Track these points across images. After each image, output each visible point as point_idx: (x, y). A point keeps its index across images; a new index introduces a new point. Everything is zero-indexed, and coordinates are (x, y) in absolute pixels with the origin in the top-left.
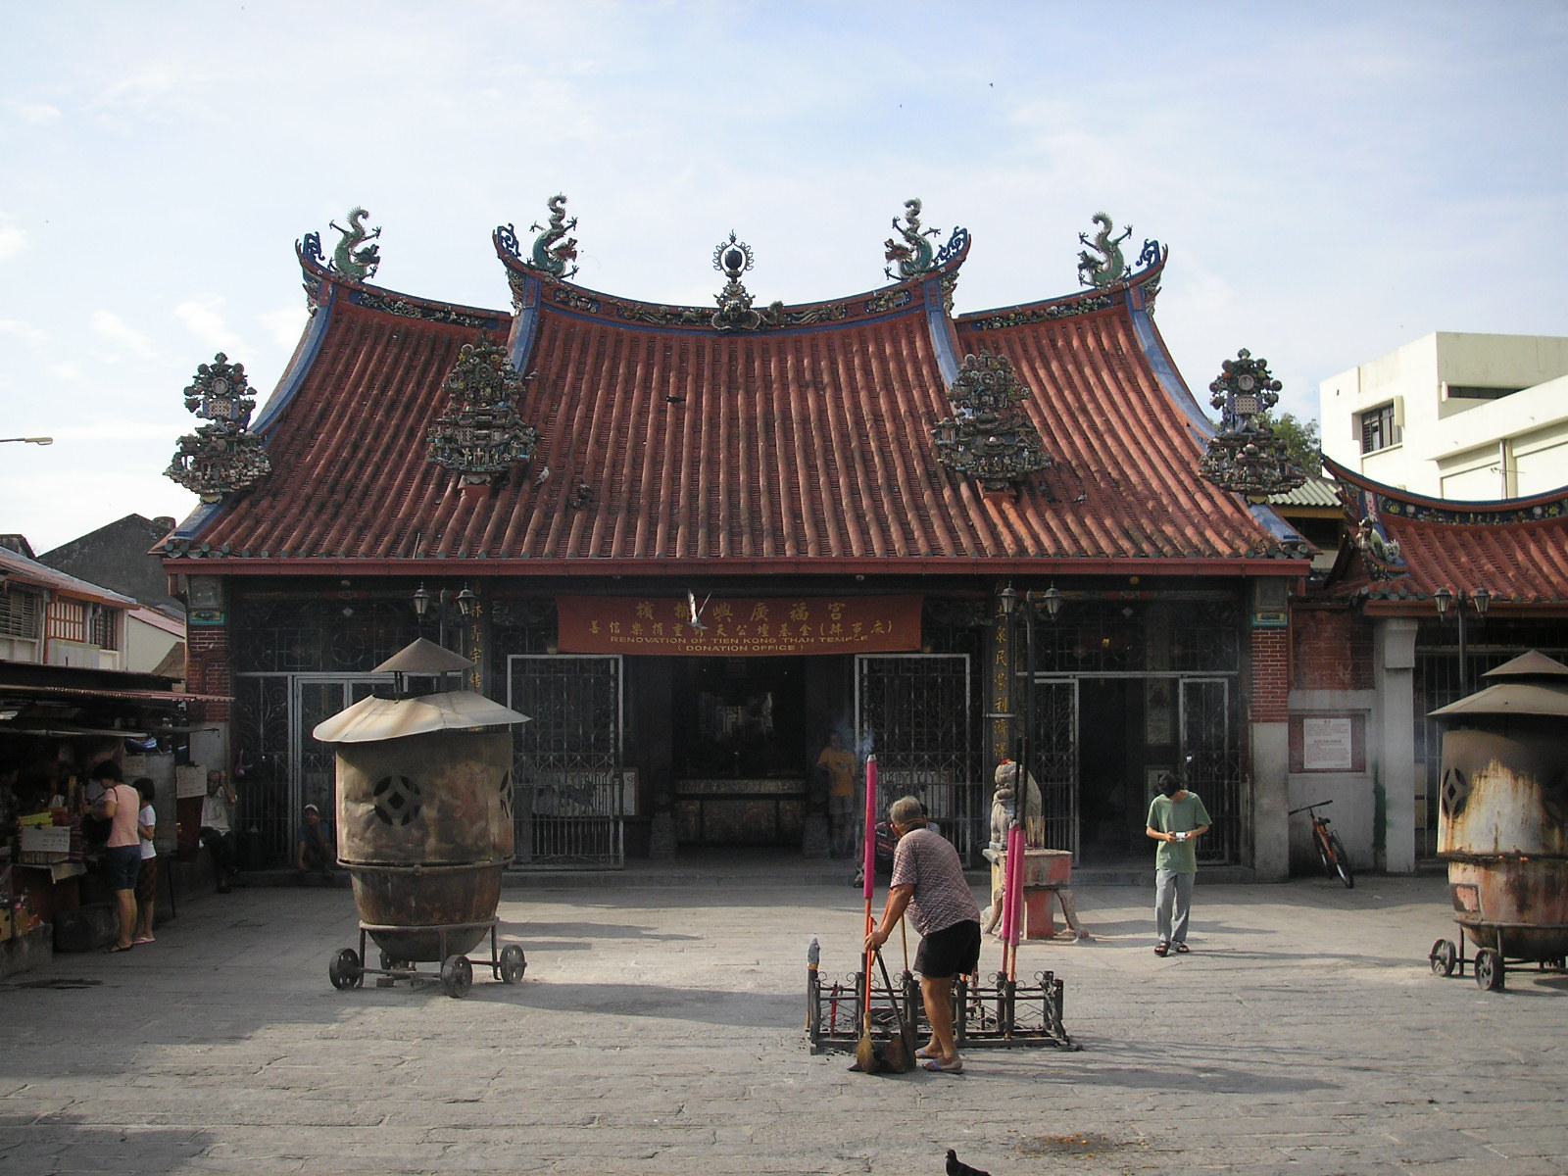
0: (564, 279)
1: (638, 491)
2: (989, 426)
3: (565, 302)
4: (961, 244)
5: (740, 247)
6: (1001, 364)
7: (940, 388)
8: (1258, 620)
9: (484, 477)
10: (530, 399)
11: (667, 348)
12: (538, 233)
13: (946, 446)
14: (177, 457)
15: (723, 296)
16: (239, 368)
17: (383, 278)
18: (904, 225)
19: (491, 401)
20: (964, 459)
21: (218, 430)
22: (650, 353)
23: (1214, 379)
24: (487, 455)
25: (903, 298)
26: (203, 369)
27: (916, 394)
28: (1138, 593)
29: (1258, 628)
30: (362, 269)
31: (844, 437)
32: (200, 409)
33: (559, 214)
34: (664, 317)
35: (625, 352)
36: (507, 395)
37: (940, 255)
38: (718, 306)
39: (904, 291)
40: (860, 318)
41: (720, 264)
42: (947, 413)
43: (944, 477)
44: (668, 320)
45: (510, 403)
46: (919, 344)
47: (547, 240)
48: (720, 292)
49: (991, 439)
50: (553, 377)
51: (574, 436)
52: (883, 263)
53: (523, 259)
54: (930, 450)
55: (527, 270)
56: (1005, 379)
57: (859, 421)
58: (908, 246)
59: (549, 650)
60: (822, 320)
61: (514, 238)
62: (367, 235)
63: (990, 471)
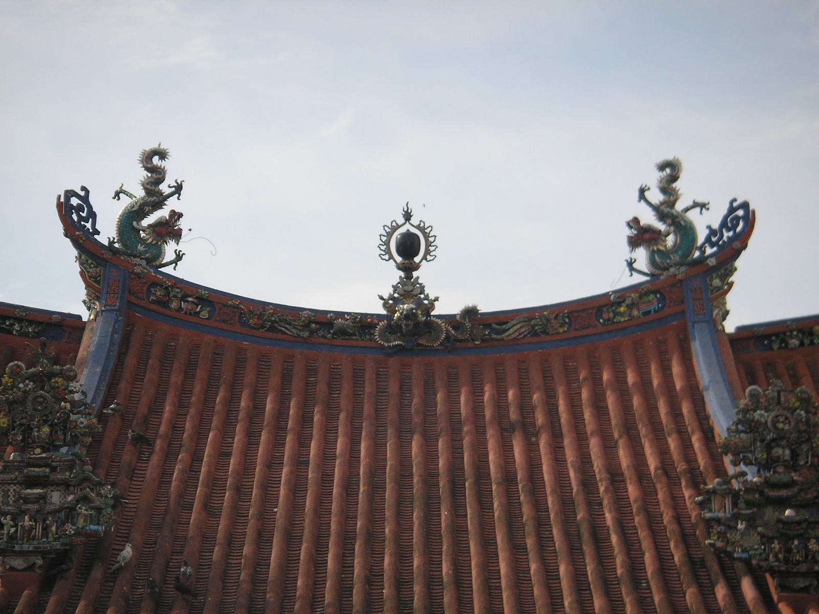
0: (162, 269)
1: (265, 581)
2: (784, 493)
3: (165, 304)
4: (740, 223)
5: (418, 227)
6: (801, 400)
7: (708, 434)
9: (32, 559)
10: (107, 444)
11: (311, 371)
12: (125, 202)
13: (718, 521)
15: (391, 297)
18: (656, 196)
19: (50, 446)
20: (746, 541)
22: (286, 378)
24: (39, 528)
25: (653, 303)
27: (672, 443)
31: (567, 504)
33: (157, 175)
34: (306, 326)
35: (249, 377)
36: (75, 438)
37: (708, 240)
38: (384, 312)
39: (655, 292)
40: (591, 331)
41: (388, 251)
42: (720, 471)
43: (715, 568)
45: (77, 449)
46: (676, 369)
48: (387, 292)
49: (787, 512)
50: (142, 409)
51: (172, 500)
52: (625, 251)
53: (103, 239)
54: (694, 527)
55: (107, 255)
56: (807, 422)
57: (588, 483)
58: (661, 226)
60: (534, 333)
61: (90, 207)
63: (787, 561)
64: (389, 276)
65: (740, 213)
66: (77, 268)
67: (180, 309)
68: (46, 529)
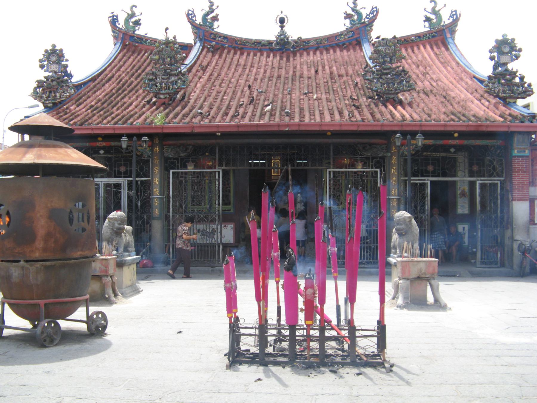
2: (387, 71)
4: (375, 13)
8: (515, 152)
12: (204, 12)
14: (35, 89)
16: (61, 50)
17: (140, 31)
21: (53, 77)
23: (491, 48)
25: (351, 34)
26: (46, 51)
28: (458, 141)
29: (515, 156)
30: (134, 28)
32: (45, 68)
34: (254, 43)
37: (366, 17)
39: (352, 31)
41: (276, 22)
44: (255, 45)
47: (207, 14)
53: (197, 22)
55: (199, 26)
58: (353, 13)
59: (189, 168)
62: (136, 15)
63: (388, 90)
64: (277, 30)
65: (375, 9)
66: (191, 30)
67: (219, 40)
68: (169, 87)
